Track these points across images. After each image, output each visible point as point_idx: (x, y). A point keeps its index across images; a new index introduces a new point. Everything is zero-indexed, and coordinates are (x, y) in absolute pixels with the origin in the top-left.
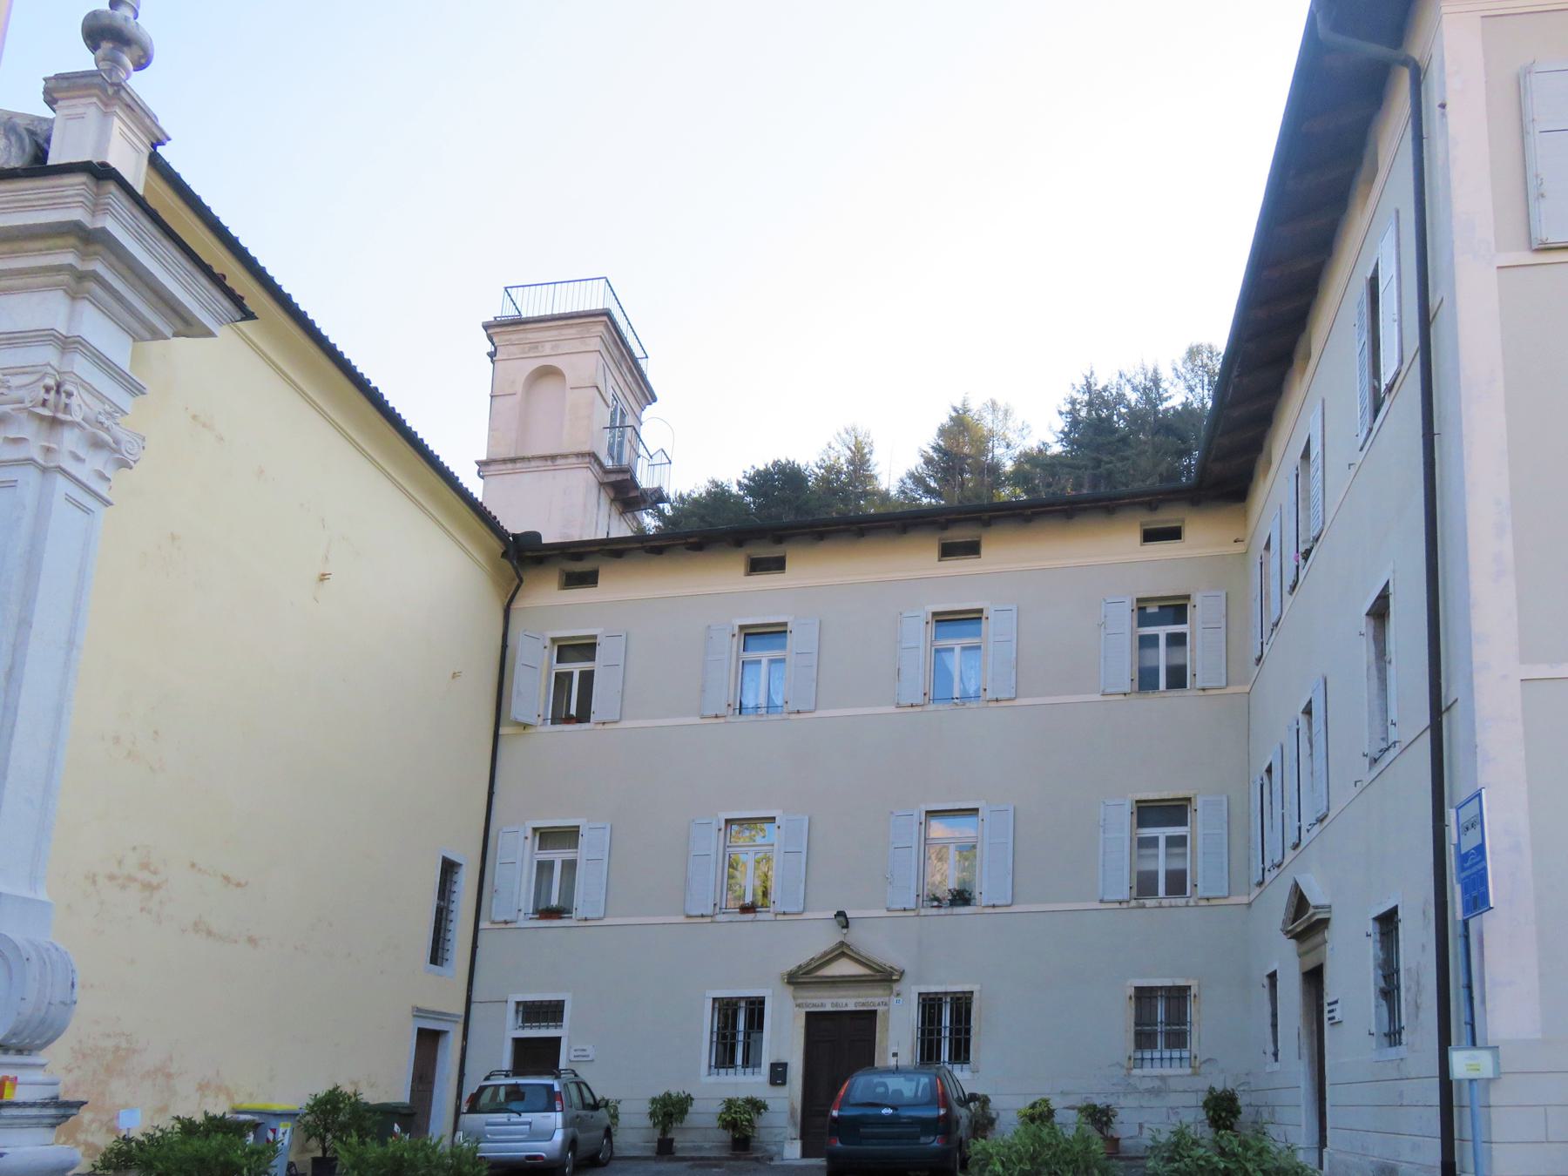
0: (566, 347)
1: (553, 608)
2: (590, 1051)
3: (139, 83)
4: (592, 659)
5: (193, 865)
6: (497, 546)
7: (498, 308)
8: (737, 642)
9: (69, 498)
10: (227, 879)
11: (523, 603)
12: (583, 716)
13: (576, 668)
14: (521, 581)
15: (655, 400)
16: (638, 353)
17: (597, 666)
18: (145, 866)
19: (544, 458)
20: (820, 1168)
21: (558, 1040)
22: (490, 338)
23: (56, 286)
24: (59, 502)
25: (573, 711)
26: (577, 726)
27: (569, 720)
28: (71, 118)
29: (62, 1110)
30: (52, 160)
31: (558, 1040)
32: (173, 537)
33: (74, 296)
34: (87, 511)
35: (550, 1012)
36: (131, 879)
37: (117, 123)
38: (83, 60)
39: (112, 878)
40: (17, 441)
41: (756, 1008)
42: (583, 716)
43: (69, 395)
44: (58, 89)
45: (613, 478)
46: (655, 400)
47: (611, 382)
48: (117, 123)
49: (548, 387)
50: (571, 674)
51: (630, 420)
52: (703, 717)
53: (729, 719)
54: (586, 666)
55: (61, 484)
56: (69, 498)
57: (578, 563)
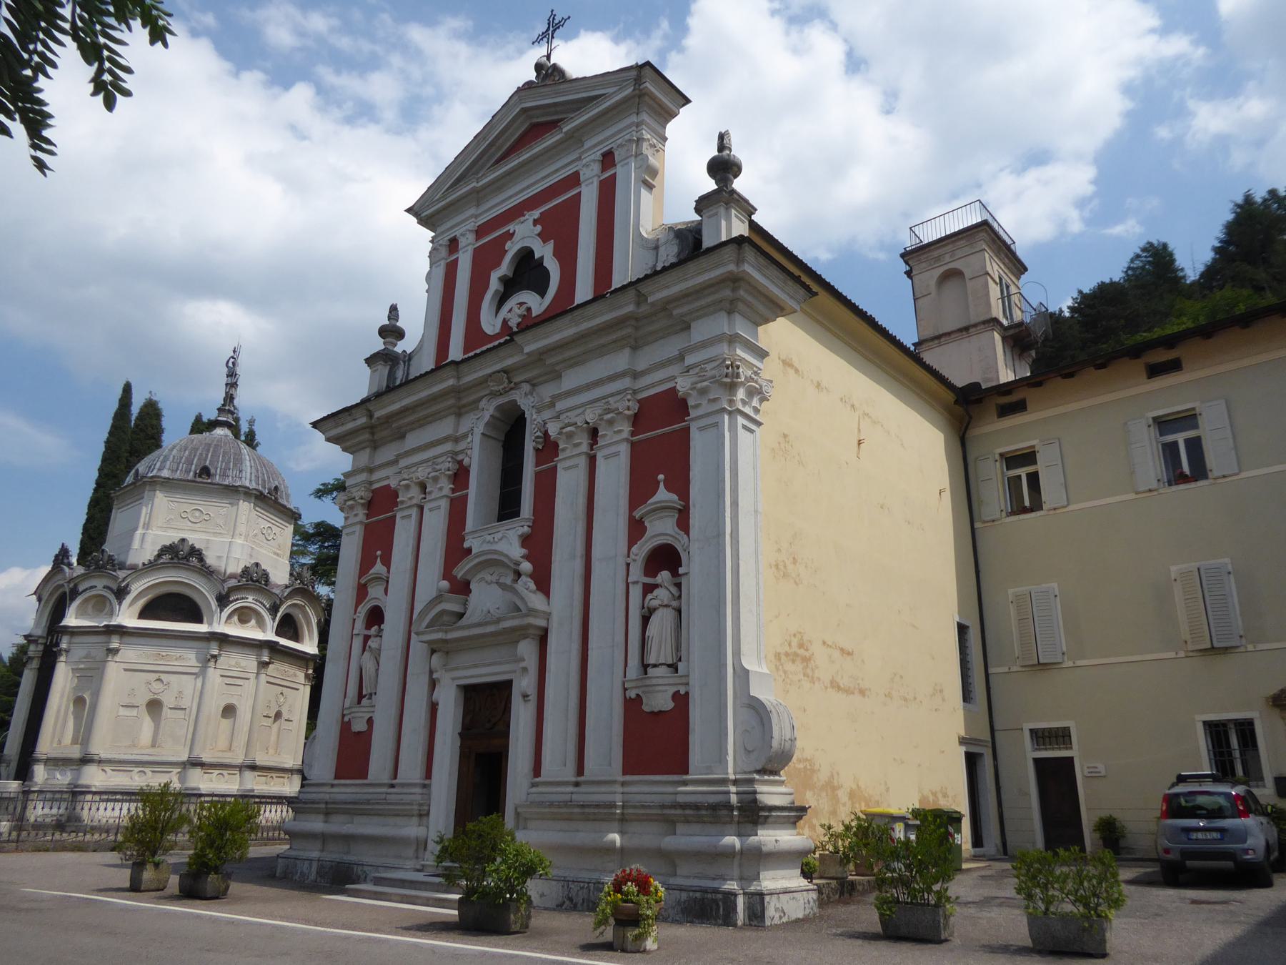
0: (959, 254)
1: (1002, 435)
2: (1101, 768)
3: (739, 184)
4: (1035, 463)
5: (824, 643)
6: (950, 397)
7: (909, 242)
8: (1154, 431)
9: (744, 427)
10: (842, 650)
11: (974, 432)
12: (1037, 505)
13: (1023, 472)
14: (971, 417)
15: (1026, 269)
16: (1009, 242)
17: (1041, 467)
18: (801, 646)
19: (960, 330)
20: (1034, 843)
21: (1072, 758)
22: (906, 263)
23: (721, 309)
24: (741, 431)
25: (1027, 503)
26: (1033, 515)
27: (1025, 510)
28: (709, 217)
29: (796, 814)
30: (707, 242)
31: (1072, 758)
32: (785, 436)
33: (730, 312)
34: (752, 431)
35: (1062, 737)
36: (796, 655)
37: (733, 211)
38: (710, 185)
39: (787, 654)
40: (715, 400)
41: (1246, 730)
42: (1037, 505)
43: (738, 367)
44: (703, 204)
45: (1012, 332)
46: (1026, 269)
47: (996, 267)
48: (733, 211)
49: (952, 288)
50: (1019, 477)
51: (1013, 289)
52: (1137, 493)
53: (1161, 491)
54: (1030, 469)
55: (741, 420)
56: (744, 427)
57: (1008, 401)
